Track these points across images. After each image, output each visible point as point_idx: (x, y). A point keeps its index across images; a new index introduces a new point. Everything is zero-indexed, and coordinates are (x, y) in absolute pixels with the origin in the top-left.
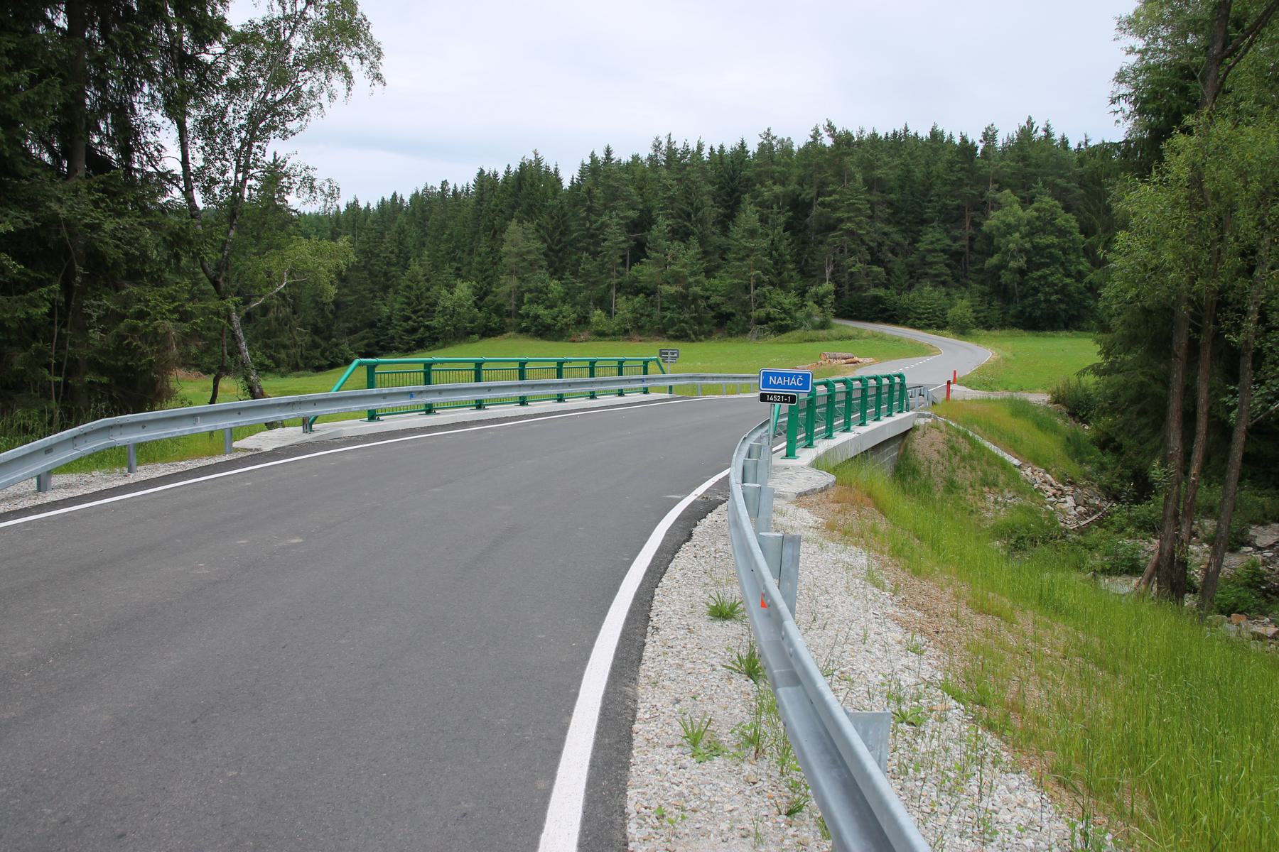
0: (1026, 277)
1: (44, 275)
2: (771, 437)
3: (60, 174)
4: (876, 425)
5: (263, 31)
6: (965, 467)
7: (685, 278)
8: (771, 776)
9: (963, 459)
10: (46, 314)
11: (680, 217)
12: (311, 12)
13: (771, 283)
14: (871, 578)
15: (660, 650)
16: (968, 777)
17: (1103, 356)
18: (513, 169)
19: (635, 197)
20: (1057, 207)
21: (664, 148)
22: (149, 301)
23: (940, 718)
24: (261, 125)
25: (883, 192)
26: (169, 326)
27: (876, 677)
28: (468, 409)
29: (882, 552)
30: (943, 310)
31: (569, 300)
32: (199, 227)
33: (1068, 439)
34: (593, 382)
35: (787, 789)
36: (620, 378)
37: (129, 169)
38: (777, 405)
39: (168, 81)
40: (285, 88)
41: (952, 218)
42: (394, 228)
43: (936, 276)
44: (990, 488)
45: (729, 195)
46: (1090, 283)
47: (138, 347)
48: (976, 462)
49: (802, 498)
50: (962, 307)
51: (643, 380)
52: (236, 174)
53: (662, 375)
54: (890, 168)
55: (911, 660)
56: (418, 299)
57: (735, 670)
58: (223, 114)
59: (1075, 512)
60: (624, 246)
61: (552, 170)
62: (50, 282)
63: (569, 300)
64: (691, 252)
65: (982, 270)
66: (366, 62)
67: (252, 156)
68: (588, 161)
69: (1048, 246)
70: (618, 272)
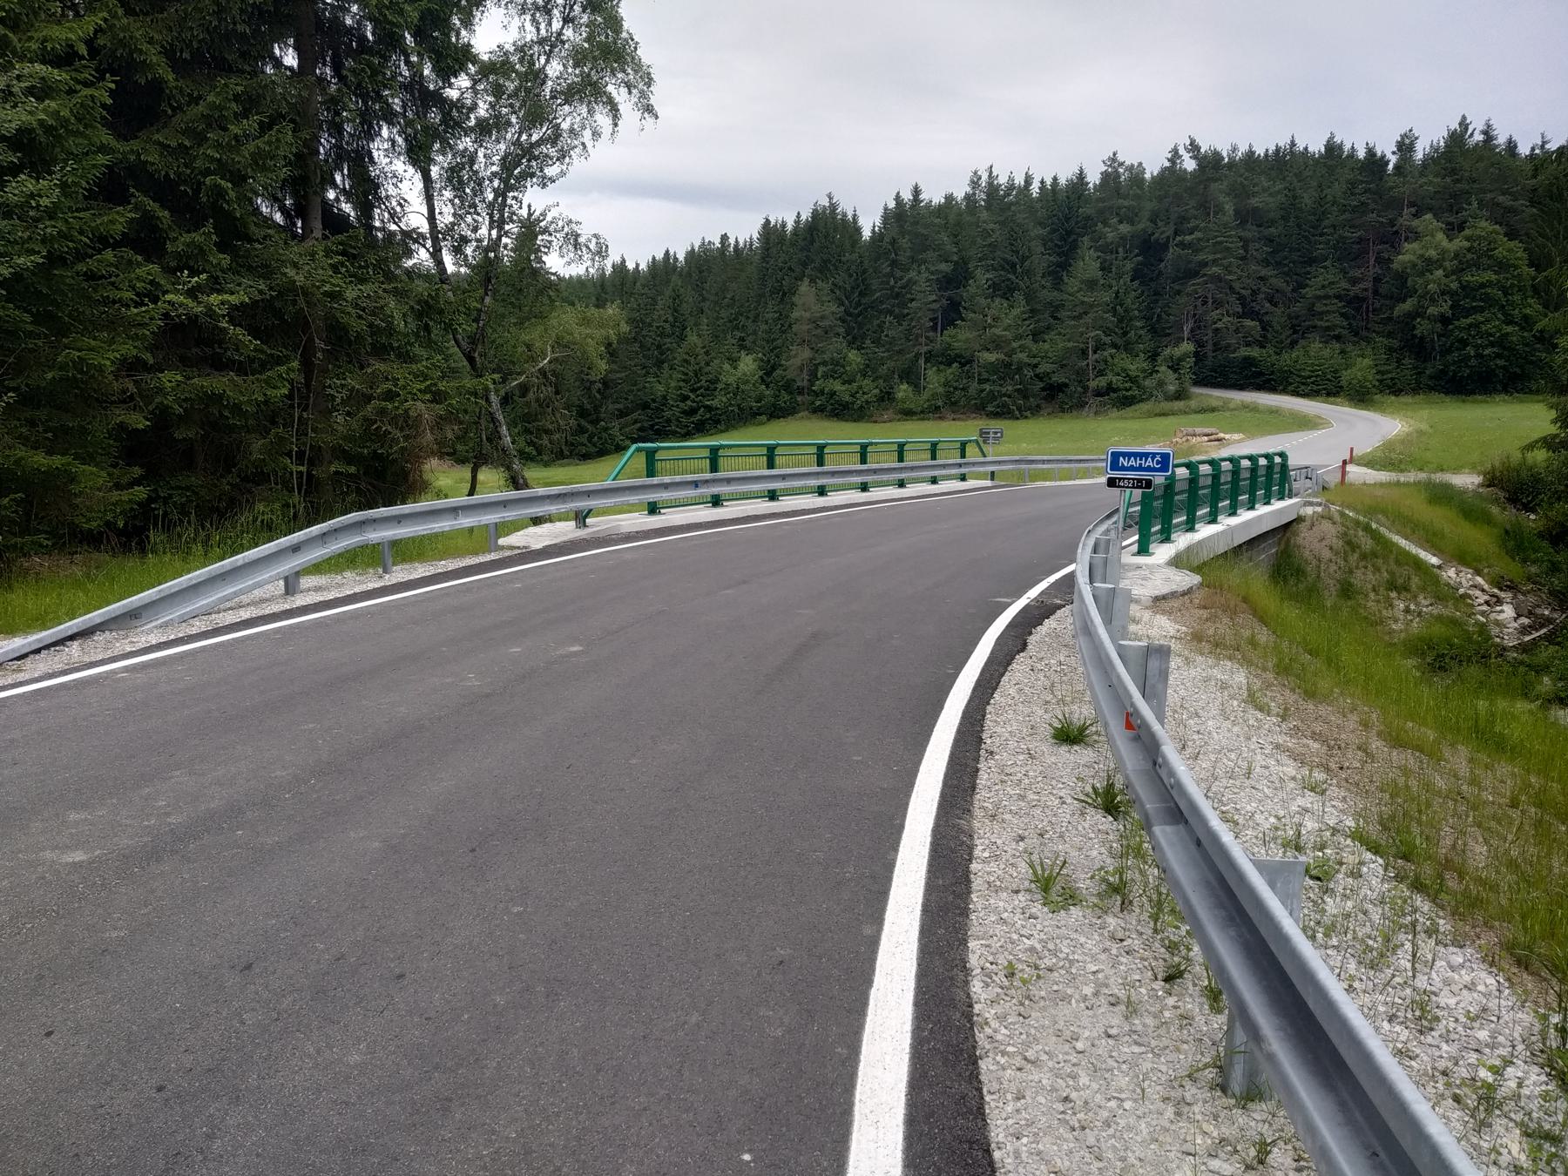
0: (1451, 327)
1: (281, 352)
2: (1121, 529)
3: (294, 236)
4: (1249, 515)
5: (514, 59)
6: (1366, 568)
7: (1008, 342)
8: (1141, 934)
9: (1364, 557)
10: (286, 396)
11: (1003, 269)
12: (569, 33)
13: (1115, 346)
14: (1252, 700)
15: (997, 778)
16: (1396, 948)
17: (1559, 424)
18: (803, 217)
19: (949, 247)
20: (1498, 233)
21: (983, 185)
22: (398, 379)
23: (1352, 873)
24: (516, 172)
25: (1260, 226)
26: (421, 409)
27: (1266, 819)
28: (759, 500)
29: (1265, 669)
30: (1336, 372)
31: (870, 373)
32: (450, 294)
33: (1507, 532)
34: (902, 468)
35: (1163, 950)
36: (934, 462)
37: (370, 228)
38: (1128, 491)
39: (409, 123)
40: (541, 125)
41: (1350, 254)
42: (668, 292)
43: (1328, 329)
44: (1399, 593)
45: (1062, 238)
46: (1541, 332)
47: (387, 433)
48: (1380, 561)
49: (1159, 602)
50: (1362, 366)
51: (960, 465)
52: (490, 231)
53: (982, 459)
54: (1271, 195)
55: (1309, 800)
56: (696, 376)
57: (1089, 804)
58: (472, 159)
59: (1516, 625)
60: (935, 306)
61: (850, 217)
62: (287, 359)
63: (870, 373)
64: (1016, 312)
65: (1390, 319)
66: (635, 91)
67: (507, 209)
68: (892, 205)
69: (1483, 286)
70: (927, 338)
